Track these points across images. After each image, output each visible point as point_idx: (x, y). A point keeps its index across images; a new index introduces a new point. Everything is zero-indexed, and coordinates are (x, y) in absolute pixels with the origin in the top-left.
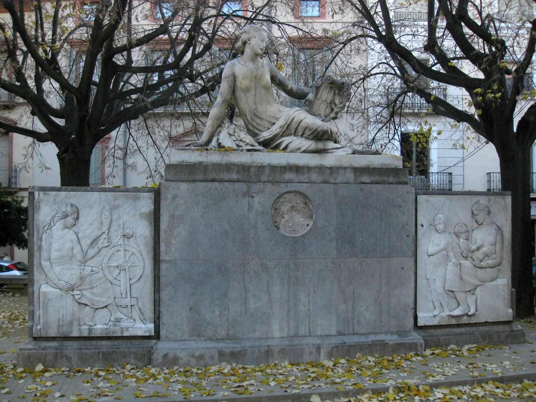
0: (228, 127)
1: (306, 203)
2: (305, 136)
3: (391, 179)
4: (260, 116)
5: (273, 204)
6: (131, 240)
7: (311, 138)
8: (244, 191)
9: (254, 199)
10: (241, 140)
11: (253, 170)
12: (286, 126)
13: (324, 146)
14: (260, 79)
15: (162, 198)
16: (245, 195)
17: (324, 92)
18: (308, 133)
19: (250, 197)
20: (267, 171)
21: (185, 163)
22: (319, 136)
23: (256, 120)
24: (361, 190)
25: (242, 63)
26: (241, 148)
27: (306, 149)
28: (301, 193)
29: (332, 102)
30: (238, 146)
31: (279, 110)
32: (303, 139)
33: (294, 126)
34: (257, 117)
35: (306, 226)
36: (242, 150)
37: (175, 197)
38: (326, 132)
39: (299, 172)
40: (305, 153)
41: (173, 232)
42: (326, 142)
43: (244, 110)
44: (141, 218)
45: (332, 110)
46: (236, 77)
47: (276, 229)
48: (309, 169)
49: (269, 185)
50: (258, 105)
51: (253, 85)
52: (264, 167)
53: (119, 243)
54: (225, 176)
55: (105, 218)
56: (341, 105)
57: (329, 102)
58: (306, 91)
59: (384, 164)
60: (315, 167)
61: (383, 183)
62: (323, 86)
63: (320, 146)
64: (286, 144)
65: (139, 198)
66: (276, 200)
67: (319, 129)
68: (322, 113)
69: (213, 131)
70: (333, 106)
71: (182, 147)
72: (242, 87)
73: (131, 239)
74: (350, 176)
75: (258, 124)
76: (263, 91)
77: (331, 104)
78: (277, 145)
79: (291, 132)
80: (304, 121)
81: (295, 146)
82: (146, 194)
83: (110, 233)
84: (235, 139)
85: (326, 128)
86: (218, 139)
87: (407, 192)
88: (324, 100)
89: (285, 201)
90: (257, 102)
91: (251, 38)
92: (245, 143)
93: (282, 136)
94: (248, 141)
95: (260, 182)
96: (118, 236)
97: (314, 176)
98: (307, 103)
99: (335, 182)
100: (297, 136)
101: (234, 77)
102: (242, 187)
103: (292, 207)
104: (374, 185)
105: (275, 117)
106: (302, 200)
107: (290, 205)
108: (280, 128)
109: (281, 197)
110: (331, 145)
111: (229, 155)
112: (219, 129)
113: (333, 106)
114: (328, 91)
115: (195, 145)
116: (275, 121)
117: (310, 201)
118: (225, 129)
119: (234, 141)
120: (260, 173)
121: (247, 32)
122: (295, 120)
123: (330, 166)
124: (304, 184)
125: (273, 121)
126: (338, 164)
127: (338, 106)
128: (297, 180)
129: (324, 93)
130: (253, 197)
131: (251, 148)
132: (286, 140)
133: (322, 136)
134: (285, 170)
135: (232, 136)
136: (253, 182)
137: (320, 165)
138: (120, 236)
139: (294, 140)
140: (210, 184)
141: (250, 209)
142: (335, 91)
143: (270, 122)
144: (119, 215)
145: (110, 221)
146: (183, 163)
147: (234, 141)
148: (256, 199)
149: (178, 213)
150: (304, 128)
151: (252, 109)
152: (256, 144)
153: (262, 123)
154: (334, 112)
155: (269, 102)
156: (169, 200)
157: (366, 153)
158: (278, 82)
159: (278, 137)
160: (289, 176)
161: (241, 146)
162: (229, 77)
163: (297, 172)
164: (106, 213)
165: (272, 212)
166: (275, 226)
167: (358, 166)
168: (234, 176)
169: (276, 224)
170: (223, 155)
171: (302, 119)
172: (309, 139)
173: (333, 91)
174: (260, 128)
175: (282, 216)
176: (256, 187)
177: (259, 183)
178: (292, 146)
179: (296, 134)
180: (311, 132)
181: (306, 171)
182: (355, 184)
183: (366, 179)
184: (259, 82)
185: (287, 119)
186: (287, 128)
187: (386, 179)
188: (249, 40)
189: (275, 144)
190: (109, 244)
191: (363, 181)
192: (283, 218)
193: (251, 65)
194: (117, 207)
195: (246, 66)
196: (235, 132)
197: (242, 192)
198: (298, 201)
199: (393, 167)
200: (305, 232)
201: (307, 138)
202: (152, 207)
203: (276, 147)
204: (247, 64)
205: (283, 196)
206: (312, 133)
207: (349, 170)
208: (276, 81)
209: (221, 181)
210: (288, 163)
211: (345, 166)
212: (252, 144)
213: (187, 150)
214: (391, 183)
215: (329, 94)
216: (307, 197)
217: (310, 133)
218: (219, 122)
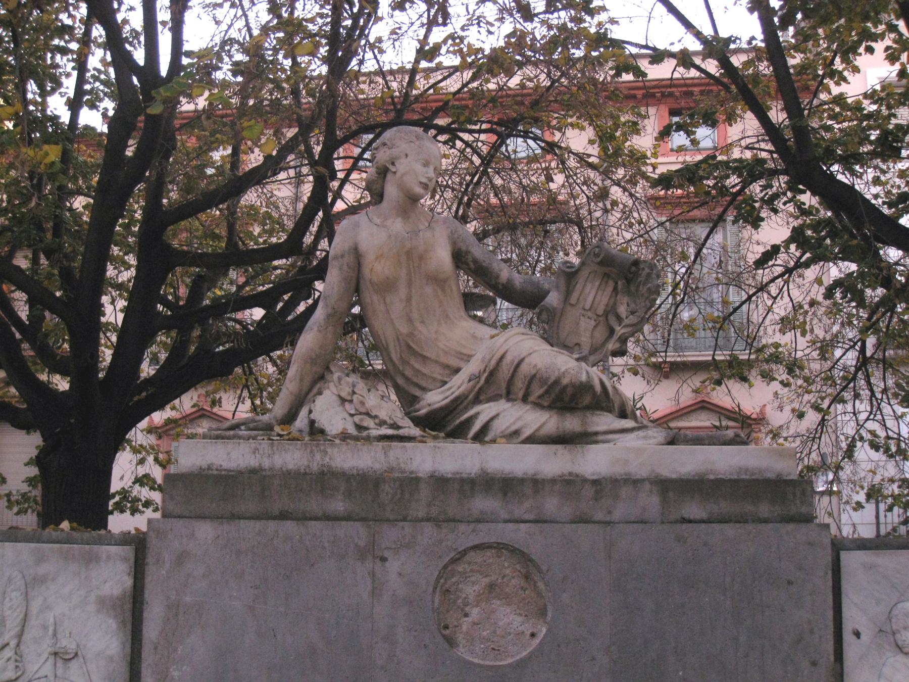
0: (340, 379)
1: (527, 577)
2: (531, 399)
3: (764, 510)
5: (437, 581)
6: (74, 664)
7: (546, 404)
8: (362, 544)
9: (387, 564)
10: (367, 414)
11: (386, 488)
12: (486, 375)
13: (584, 423)
14: (421, 258)
15: (150, 559)
16: (362, 554)
17: (589, 285)
18: (537, 391)
19: (378, 561)
20: (424, 492)
21: (215, 472)
22: (567, 399)
24: (679, 539)
25: (378, 221)
26: (365, 434)
27: (534, 433)
28: (514, 551)
29: (611, 311)
30: (359, 427)
31: (474, 337)
32: (528, 407)
33: (505, 373)
34: (415, 353)
35: (528, 637)
36: (368, 439)
37: (181, 558)
38: (585, 387)
39: (510, 494)
40: (533, 443)
41: (175, 650)
42: (588, 414)
43: (382, 338)
44: (98, 611)
45: (612, 331)
46: (361, 255)
47: (446, 645)
48: (536, 484)
49: (428, 529)
50: (418, 324)
51: (403, 273)
52: (417, 480)
53: (42, 673)
54: (314, 505)
55: (10, 608)
56: (633, 319)
57: (600, 311)
58: (546, 286)
59: (747, 470)
60: (553, 481)
61: (742, 520)
62: (585, 273)
63: (572, 424)
64: (487, 418)
65: (97, 559)
66: (445, 567)
67: (565, 381)
68: (585, 340)
69: (300, 390)
70: (613, 320)
71: (216, 433)
72: (375, 279)
73: (73, 662)
74: (651, 502)
75: (418, 371)
76: (429, 290)
77: (606, 314)
78: (462, 423)
79: (499, 392)
80: (527, 360)
81: (504, 427)
82: (113, 549)
83: (22, 647)
84: (353, 412)
85: (584, 378)
86: (310, 412)
87: (809, 543)
88: (587, 307)
89: (472, 571)
90: (415, 315)
91: (398, 158)
92: (377, 421)
93: (477, 400)
94: (383, 415)
95: (404, 519)
96: (40, 655)
97: (551, 504)
98: (544, 316)
99: (608, 519)
100: (515, 400)
101: (357, 254)
102: (357, 533)
103: (491, 586)
104: (716, 526)
105: (461, 353)
106: (518, 567)
107: (486, 581)
108: (470, 381)
109: (459, 559)
110: (604, 421)
112: (318, 386)
113: (613, 320)
114: (597, 284)
115: (251, 425)
116: (462, 364)
117: (540, 571)
118: (331, 385)
119: (352, 415)
120: (407, 496)
121: (388, 143)
122: (508, 358)
123: (595, 477)
124: (522, 525)
125: (454, 362)
126: (618, 470)
127: (626, 322)
128: (504, 515)
129: (587, 290)
130: (384, 559)
131: (390, 432)
132: (485, 411)
133: (573, 397)
134: (472, 489)
135: (347, 404)
136: (388, 520)
137: (570, 474)
138: (46, 655)
139: (505, 410)
140: (272, 525)
141: (376, 592)
142: (616, 283)
143: (447, 367)
144: (45, 599)
145: (22, 616)
146: (210, 472)
147: (352, 415)
148: (394, 565)
149: (188, 599)
150: (528, 379)
151: (401, 334)
152: (407, 422)
153: (425, 370)
154: (615, 337)
155: (447, 316)
156: (167, 565)
157: (707, 442)
158: (472, 266)
159: (465, 404)
160: (483, 504)
161: (367, 429)
162: (342, 256)
163: (505, 494)
164: (14, 594)
165: (437, 601)
166: (444, 636)
167: (674, 476)
168: (338, 505)
169: (447, 632)
170: (312, 451)
171: (522, 356)
172: (542, 407)
173: (611, 284)
174: (423, 383)
175: (462, 610)
176: (390, 535)
177: (401, 524)
178: (499, 426)
179: (511, 397)
180: (546, 387)
181: (527, 489)
182: (663, 523)
183: (694, 509)
185: (488, 357)
186: (487, 381)
187: (749, 508)
188: (393, 164)
189: (458, 422)
190: (19, 673)
191: (686, 516)
192: (466, 615)
193: (398, 225)
194: (40, 581)
195: (385, 227)
196: (354, 393)
197: (356, 545)
198: (507, 572)
199: (770, 475)
200: (524, 654)
201: (538, 405)
202: (129, 582)
203: (458, 433)
204: (389, 223)
205: (467, 558)
206: (547, 392)
207: (647, 486)
208: (467, 264)
209: (304, 518)
211: (638, 477)
212: (395, 423)
213: (229, 438)
214: (766, 521)
215: (600, 293)
216: (531, 560)
217: (541, 392)
218: (318, 369)
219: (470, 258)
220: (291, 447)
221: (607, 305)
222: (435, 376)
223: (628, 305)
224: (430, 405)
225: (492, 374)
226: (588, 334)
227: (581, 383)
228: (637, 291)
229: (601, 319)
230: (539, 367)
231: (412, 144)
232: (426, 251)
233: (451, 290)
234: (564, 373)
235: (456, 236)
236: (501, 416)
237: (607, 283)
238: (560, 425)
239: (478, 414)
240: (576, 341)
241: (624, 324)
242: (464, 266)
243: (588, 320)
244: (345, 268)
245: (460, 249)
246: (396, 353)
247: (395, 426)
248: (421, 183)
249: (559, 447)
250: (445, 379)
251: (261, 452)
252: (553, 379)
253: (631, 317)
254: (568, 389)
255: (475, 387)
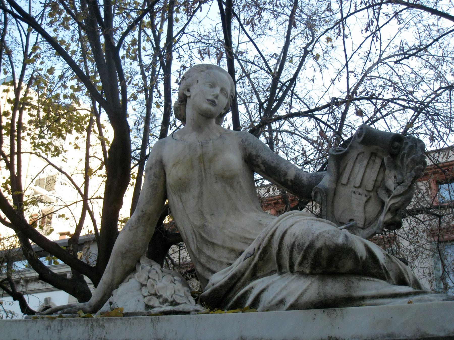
4: (210, 240)
14: (211, 161)
17: (358, 166)
22: (324, 263)
23: (205, 250)
27: (296, 301)
30: (148, 307)
32: (294, 277)
45: (383, 203)
50: (208, 217)
56: (400, 189)
57: (370, 187)
67: (319, 244)
69: (112, 280)
70: (382, 194)
75: (209, 257)
76: (218, 187)
77: (376, 188)
78: (239, 298)
80: (289, 232)
88: (358, 185)
93: (254, 276)
94: (167, 294)
105: (246, 238)
111: (106, 325)
114: (365, 163)
125: (238, 246)
127: (395, 193)
129: (356, 169)
139: (274, 282)
143: (232, 250)
154: (386, 209)
155: (236, 209)
158: (263, 168)
159: (242, 280)
161: (153, 307)
167: (442, 334)
170: (92, 327)
173: (378, 162)
178: (266, 299)
180: (302, 253)
184: (210, 168)
186: (261, 258)
188: (188, 90)
189: (236, 297)
201: (302, 274)
206: (304, 258)
208: (259, 166)
210: (325, 296)
219: (260, 161)
220: (75, 323)
221: (376, 181)
222: (222, 260)
223: (395, 177)
224: (213, 285)
225: (266, 250)
226: (361, 209)
227: (337, 245)
228: (402, 163)
229: (372, 194)
230: (297, 234)
231: (202, 73)
232: (216, 155)
233: (241, 187)
234: (317, 237)
235: (246, 143)
236: (270, 288)
237: (374, 161)
238: (321, 290)
239: (252, 288)
240: (350, 218)
241: (392, 195)
242: (256, 169)
243: (359, 196)
244: (152, 177)
245: (250, 154)
246: (194, 243)
247: (174, 303)
248: (208, 100)
249: (318, 312)
250: (231, 262)
251: (52, 328)
252: (307, 243)
253: (399, 187)
254: (323, 252)
255: (250, 264)
